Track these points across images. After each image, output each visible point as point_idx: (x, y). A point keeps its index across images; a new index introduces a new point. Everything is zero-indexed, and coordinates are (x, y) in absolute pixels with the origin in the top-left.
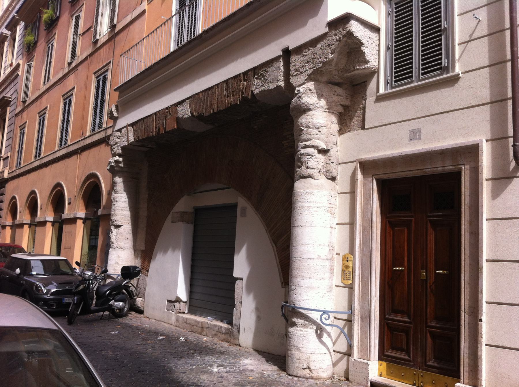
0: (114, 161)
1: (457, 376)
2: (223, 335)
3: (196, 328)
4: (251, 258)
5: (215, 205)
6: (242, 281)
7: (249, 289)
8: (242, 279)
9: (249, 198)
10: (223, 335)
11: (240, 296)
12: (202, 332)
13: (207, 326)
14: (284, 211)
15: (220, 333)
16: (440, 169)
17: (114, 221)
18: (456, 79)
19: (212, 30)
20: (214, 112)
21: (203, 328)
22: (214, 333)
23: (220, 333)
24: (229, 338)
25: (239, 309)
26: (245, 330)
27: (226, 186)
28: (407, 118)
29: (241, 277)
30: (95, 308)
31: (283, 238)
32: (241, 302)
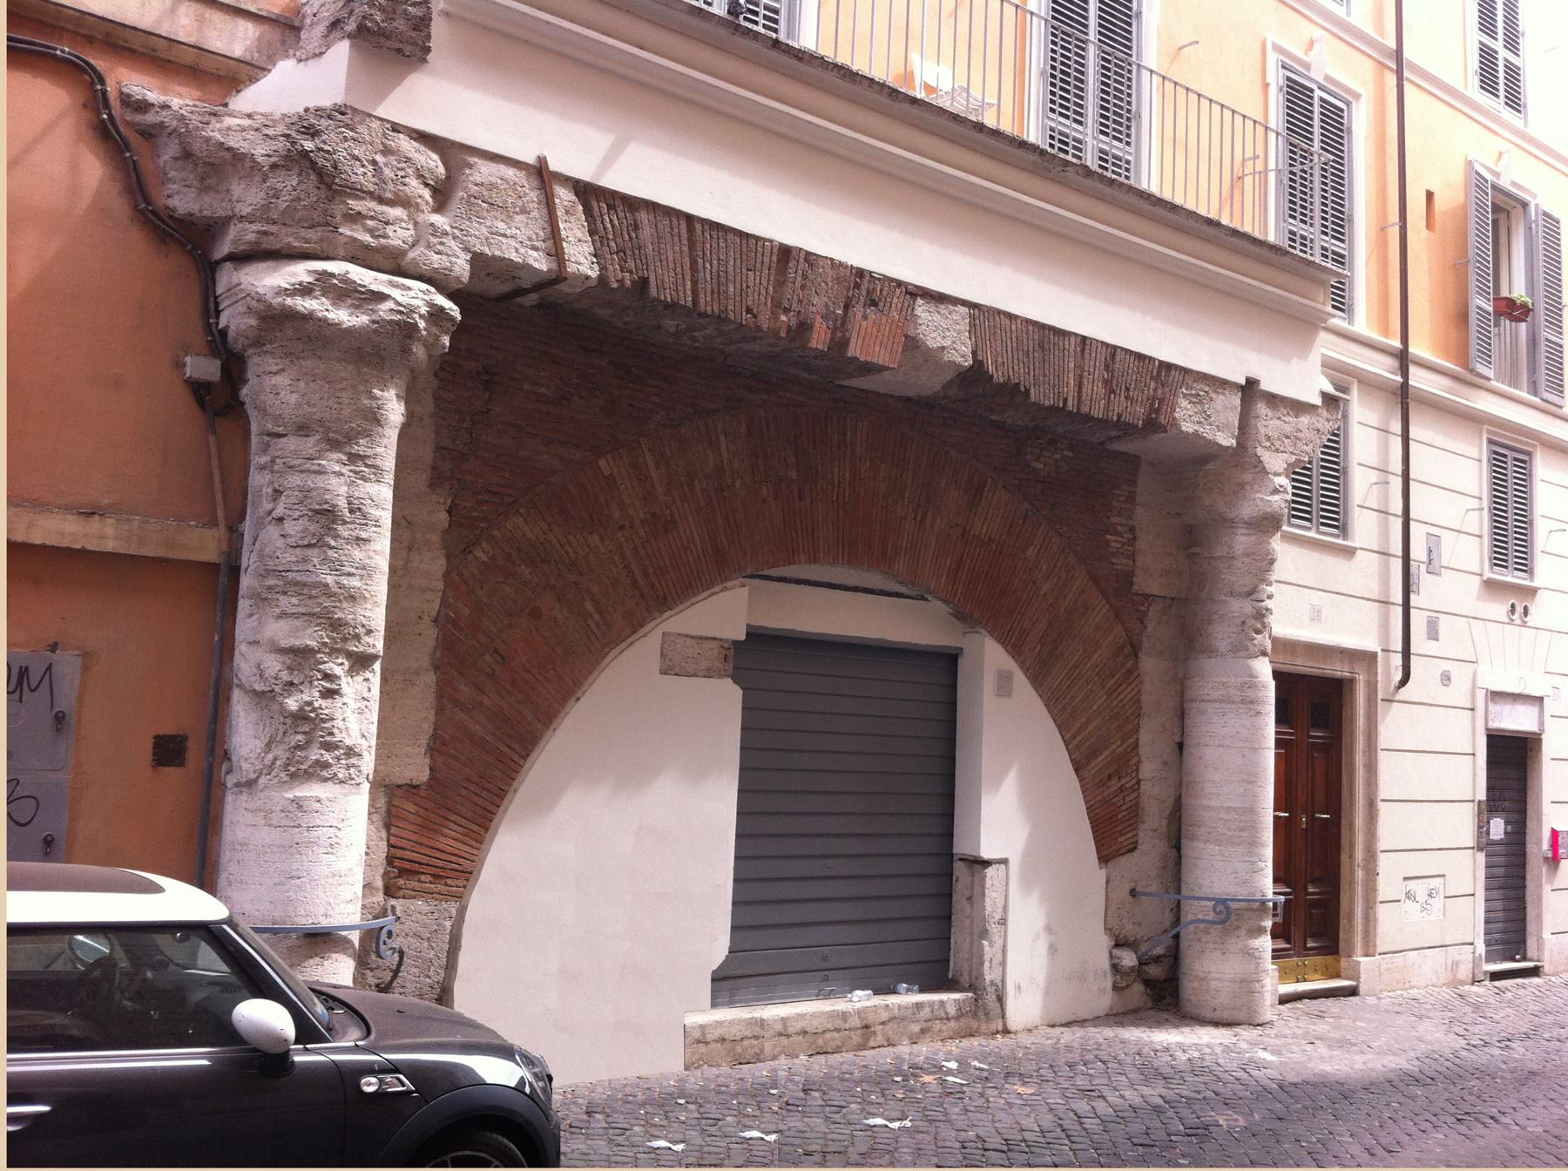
0: (424, 310)
1: (10, 1051)
2: (952, 1021)
3: (836, 1035)
4: (1033, 803)
5: (916, 644)
6: (1003, 866)
7: (1027, 883)
8: (1005, 862)
9: (1015, 649)
10: (952, 1021)
11: (1000, 905)
12: (868, 1039)
13: (885, 1016)
14: (1105, 697)
15: (941, 1019)
16: (1339, 673)
17: (360, 630)
18: (1350, 552)
19: (1102, 182)
20: (1078, 409)
21: (867, 1027)
22: (916, 1028)
23: (941, 1019)
24: (974, 1024)
25: (999, 942)
26: (1019, 987)
27: (895, 587)
28: (1307, 584)
29: (1003, 856)
30: (1047, 1039)
31: (1100, 758)
32: (1003, 922)
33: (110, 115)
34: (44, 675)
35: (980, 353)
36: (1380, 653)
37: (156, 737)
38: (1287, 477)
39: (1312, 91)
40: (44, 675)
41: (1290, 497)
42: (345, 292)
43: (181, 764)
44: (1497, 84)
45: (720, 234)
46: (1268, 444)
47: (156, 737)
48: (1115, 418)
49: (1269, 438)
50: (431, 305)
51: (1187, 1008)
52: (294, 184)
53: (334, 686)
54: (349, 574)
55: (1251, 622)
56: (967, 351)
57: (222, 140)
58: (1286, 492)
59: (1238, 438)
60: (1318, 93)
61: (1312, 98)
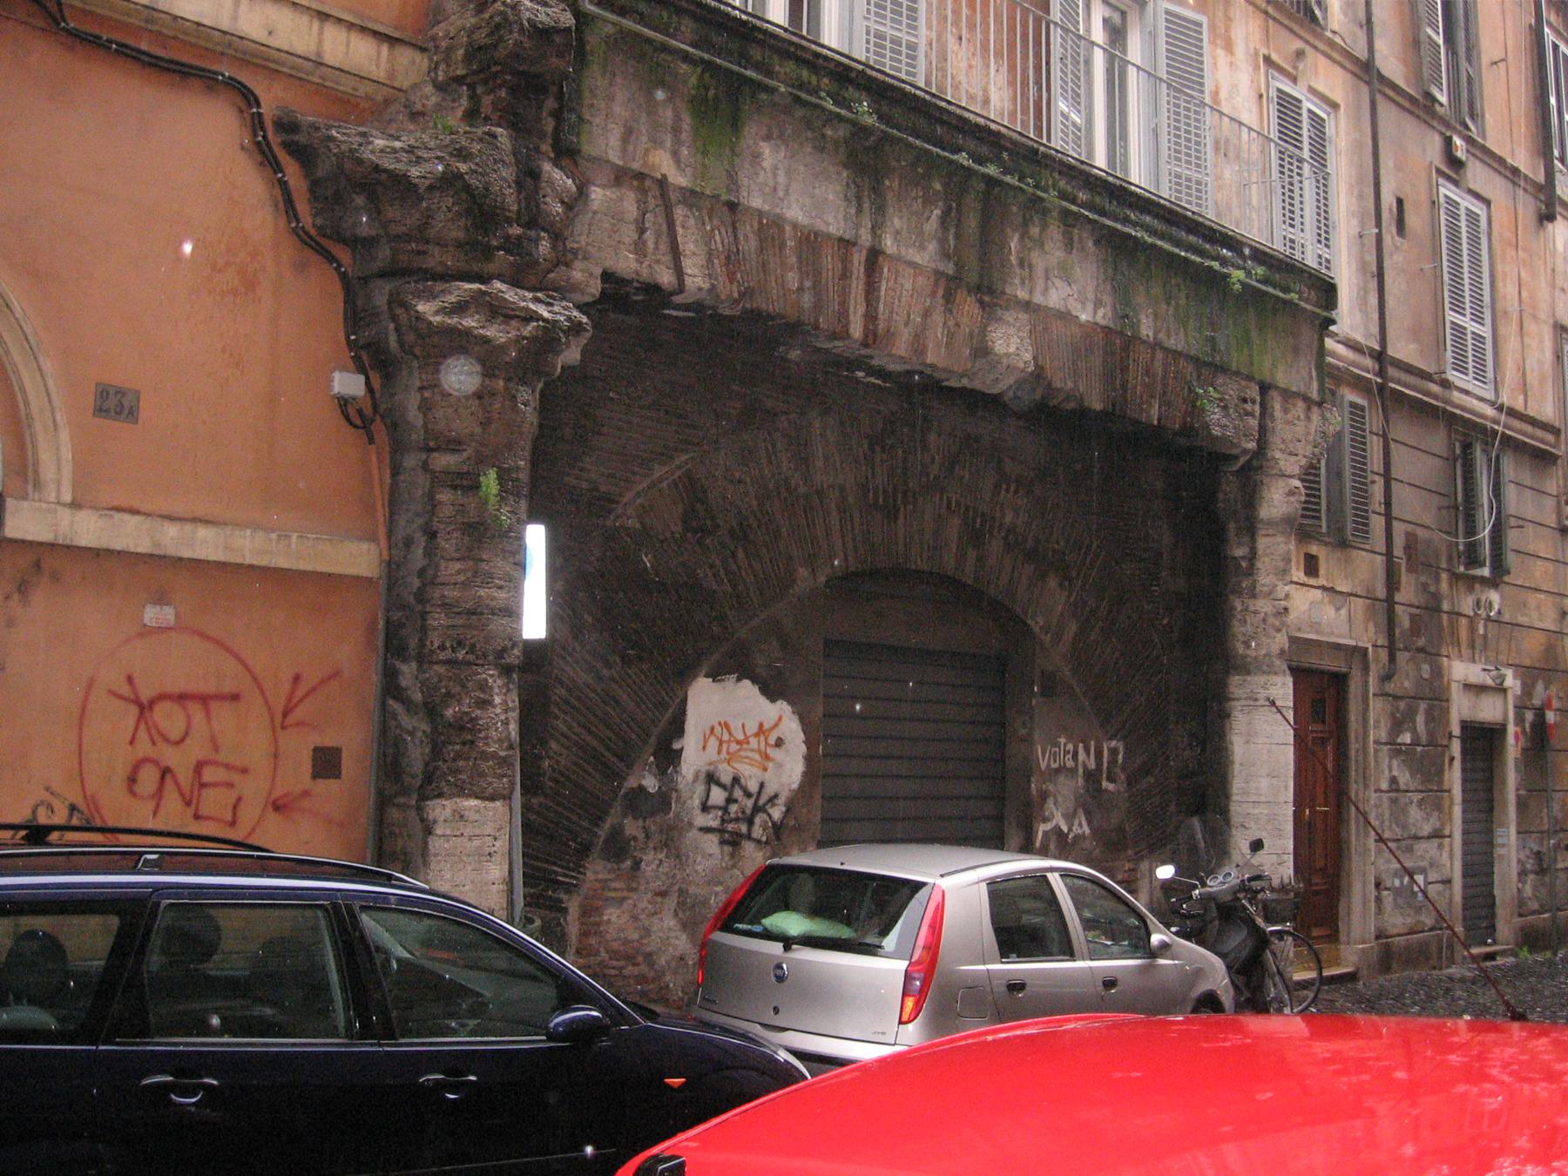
33: (264, 137)
34: (301, 700)
35: (1040, 358)
36: (1370, 649)
37: (316, 750)
38: (1302, 480)
39: (1300, 101)
40: (301, 700)
41: (1303, 499)
42: (497, 311)
43: (338, 776)
44: (1300, 122)
45: (1246, 156)
46: (1283, 447)
47: (316, 750)
48: (1155, 422)
49: (1283, 441)
50: (569, 319)
51: (30, 817)
52: (450, 205)
53: (487, 697)
54: (500, 588)
55: (1271, 620)
56: (1028, 356)
57: (377, 161)
58: (1300, 494)
59: (1259, 441)
60: (1307, 105)
61: (1300, 108)
